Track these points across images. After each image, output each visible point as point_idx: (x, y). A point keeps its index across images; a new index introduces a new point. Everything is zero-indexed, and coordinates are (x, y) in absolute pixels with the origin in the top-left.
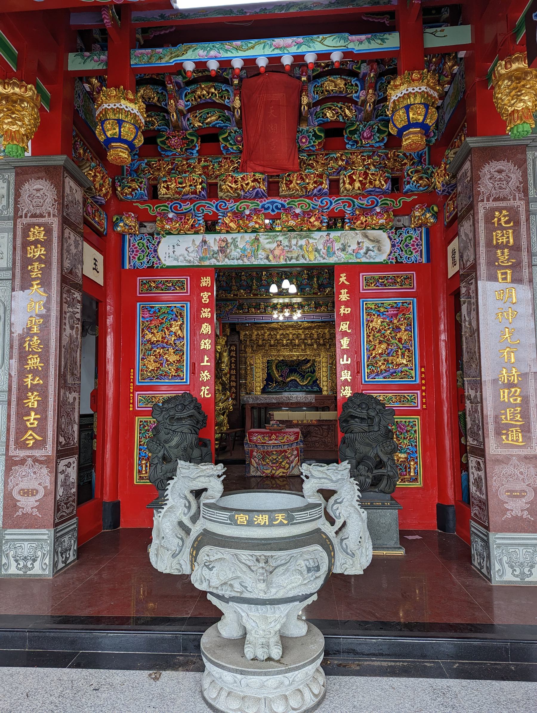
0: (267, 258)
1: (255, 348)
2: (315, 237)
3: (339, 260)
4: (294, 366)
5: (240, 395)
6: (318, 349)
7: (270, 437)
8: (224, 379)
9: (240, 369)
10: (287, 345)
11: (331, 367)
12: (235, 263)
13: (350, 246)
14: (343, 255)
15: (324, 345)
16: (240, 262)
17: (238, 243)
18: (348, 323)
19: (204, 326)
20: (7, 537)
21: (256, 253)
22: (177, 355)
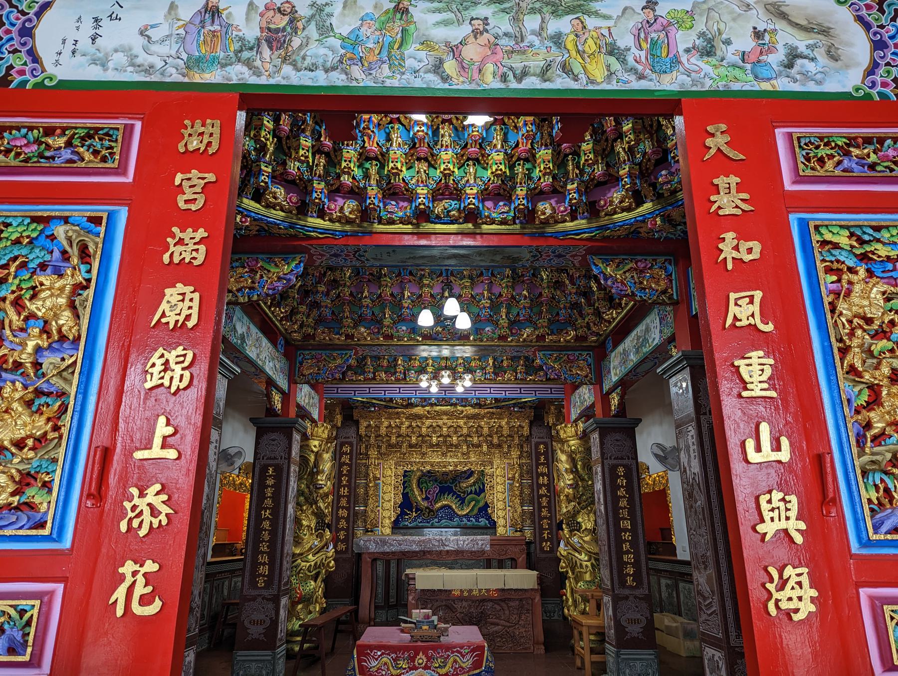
0: (437, 68)
1: (383, 450)
2: (604, 11)
3: (694, 82)
4: (447, 483)
5: (354, 534)
6: (489, 453)
7: (412, 659)
8: (321, 505)
9: (357, 486)
10: (437, 445)
11: (511, 485)
12: (321, 79)
13: (728, 42)
14: (707, 69)
15: (499, 446)
16: (338, 79)
17: (334, 21)
18: (758, 295)
19: (171, 294)
20: (239, 658)
21: (395, 52)
22: (39, 412)
